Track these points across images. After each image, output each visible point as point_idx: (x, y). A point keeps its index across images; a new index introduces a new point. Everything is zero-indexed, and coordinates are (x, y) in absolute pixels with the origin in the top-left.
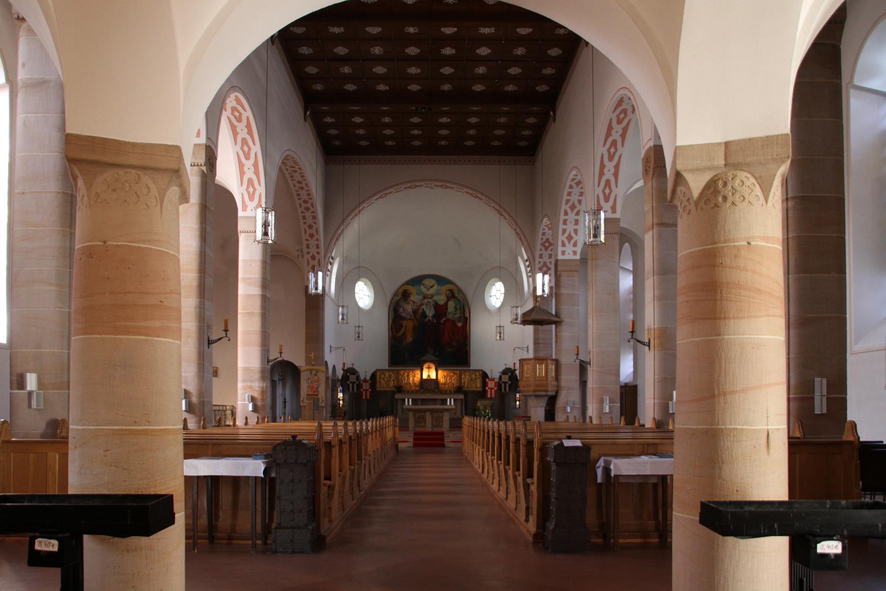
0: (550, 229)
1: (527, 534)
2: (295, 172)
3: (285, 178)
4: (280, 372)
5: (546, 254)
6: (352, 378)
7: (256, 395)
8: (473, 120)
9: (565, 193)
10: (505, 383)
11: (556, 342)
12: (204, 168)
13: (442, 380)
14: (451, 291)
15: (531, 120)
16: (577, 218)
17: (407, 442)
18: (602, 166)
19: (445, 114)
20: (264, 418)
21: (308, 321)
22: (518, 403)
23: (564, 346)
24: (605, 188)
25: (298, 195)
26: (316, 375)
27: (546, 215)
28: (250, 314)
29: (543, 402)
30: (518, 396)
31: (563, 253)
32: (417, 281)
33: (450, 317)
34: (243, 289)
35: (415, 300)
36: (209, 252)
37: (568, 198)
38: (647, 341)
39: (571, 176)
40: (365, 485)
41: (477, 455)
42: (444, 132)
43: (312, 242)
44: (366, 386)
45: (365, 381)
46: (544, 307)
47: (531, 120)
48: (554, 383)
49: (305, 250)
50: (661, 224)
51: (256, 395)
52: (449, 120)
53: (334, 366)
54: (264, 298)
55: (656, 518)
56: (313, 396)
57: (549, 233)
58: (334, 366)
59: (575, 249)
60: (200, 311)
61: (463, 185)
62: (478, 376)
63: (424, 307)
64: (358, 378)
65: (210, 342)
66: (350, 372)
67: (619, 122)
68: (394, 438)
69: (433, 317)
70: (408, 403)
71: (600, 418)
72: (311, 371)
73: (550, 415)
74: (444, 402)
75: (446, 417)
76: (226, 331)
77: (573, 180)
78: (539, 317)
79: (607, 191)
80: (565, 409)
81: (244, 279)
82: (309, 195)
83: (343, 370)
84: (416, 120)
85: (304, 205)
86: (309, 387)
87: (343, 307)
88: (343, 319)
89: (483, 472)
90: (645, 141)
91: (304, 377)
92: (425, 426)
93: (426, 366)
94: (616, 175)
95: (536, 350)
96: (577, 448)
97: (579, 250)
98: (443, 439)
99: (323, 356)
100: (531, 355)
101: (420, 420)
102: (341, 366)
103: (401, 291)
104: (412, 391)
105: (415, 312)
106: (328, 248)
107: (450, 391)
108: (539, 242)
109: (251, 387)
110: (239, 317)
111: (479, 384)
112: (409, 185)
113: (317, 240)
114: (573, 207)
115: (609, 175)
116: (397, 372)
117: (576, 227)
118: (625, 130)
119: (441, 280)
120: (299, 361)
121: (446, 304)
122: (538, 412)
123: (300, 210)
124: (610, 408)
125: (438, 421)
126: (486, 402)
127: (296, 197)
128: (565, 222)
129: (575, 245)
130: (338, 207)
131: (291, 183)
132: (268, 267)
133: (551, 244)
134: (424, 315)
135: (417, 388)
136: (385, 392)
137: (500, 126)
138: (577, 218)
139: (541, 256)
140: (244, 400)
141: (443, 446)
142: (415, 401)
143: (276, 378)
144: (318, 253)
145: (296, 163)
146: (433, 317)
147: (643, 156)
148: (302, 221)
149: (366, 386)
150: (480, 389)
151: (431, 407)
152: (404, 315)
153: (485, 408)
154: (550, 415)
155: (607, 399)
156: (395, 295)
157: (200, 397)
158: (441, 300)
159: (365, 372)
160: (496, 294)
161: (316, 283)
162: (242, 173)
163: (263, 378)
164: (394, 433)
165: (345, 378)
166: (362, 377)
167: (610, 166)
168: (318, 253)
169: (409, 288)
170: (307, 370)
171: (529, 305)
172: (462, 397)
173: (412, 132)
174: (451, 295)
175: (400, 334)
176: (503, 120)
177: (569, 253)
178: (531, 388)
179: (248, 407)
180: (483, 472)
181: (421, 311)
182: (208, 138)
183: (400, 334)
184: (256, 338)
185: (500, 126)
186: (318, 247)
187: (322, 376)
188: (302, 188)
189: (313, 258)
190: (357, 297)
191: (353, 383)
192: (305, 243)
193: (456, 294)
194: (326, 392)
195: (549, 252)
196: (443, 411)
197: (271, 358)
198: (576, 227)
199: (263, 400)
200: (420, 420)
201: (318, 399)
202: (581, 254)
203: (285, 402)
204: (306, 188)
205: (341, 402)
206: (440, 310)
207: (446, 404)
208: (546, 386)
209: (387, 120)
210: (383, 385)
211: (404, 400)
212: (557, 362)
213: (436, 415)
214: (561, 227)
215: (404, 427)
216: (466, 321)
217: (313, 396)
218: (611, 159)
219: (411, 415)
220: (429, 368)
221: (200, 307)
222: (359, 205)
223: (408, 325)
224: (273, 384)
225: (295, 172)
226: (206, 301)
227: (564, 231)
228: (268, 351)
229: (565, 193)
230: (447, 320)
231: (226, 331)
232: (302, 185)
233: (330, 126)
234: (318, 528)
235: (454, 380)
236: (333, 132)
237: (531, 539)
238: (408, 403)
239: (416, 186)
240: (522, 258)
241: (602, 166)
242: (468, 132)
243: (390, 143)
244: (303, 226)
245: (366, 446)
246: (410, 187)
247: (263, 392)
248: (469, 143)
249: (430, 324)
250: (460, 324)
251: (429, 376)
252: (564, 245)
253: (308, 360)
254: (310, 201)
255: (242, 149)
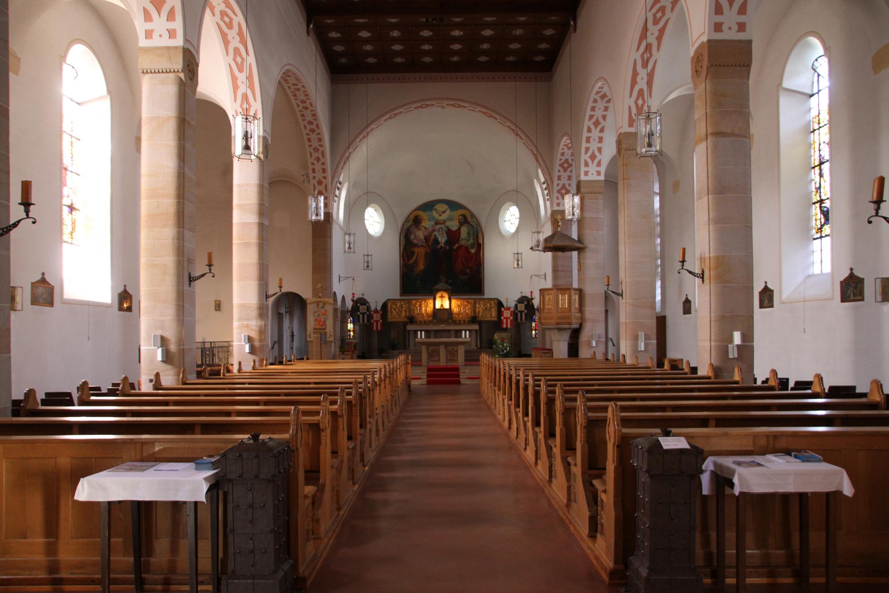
0: (569, 149)
1: (599, 569)
2: (298, 90)
3: (286, 94)
4: (285, 306)
5: (565, 175)
6: (363, 309)
7: (254, 335)
8: (488, 33)
9: (589, 108)
10: (521, 312)
11: (579, 270)
12: (182, 75)
13: (455, 309)
14: (464, 216)
15: (549, 32)
16: (601, 135)
17: (420, 382)
18: (635, 74)
19: (457, 26)
20: (261, 361)
21: (314, 250)
22: (534, 332)
23: (588, 273)
24: (637, 99)
25: (303, 115)
26: (323, 308)
27: (566, 134)
28: (247, 245)
29: (566, 336)
30: (534, 325)
31: (586, 173)
32: (429, 206)
33: (462, 243)
34: (238, 217)
35: (427, 226)
36: (189, 173)
37: (592, 113)
38: (697, 271)
39: (596, 89)
40: (370, 456)
41: (502, 405)
42: (456, 47)
43: (318, 167)
44: (377, 317)
45: (376, 311)
46: (565, 232)
47: (549, 32)
48: (579, 315)
49: (311, 175)
50: (717, 134)
51: (254, 335)
52: (462, 33)
53: (343, 297)
54: (261, 226)
55: (787, 544)
56: (321, 330)
57: (568, 153)
58: (343, 297)
59: (598, 169)
60: (179, 243)
61: (475, 103)
62: (493, 305)
63: (436, 233)
64: (368, 308)
65: (191, 279)
66: (360, 302)
67: (656, 22)
68: (406, 378)
69: (445, 244)
70: (421, 336)
71: (637, 357)
72: (318, 303)
73: (573, 350)
74: (458, 333)
75: (461, 351)
76: (210, 265)
77: (598, 93)
78: (558, 245)
79: (640, 102)
80: (590, 343)
81: (240, 206)
82: (314, 115)
83: (353, 301)
84: (426, 33)
85: (309, 127)
86: (316, 320)
87: (349, 234)
88: (350, 248)
89: (510, 428)
90: (696, 34)
91: (310, 309)
92: (439, 360)
93: (439, 295)
94: (650, 83)
95: (555, 277)
96: (682, 451)
97: (603, 169)
98: (458, 376)
99: (331, 287)
100: (549, 284)
101: (433, 354)
102: (351, 297)
103: (412, 217)
104: (425, 322)
105: (427, 239)
106: (335, 173)
107: (464, 321)
108: (558, 162)
109: (247, 326)
110: (235, 248)
111: (494, 313)
112: (419, 105)
113: (323, 164)
114: (597, 124)
115: (642, 84)
116: (409, 301)
117: (600, 145)
118: (662, 32)
119: (453, 205)
120: (306, 293)
121: (459, 229)
122: (561, 348)
123: (304, 132)
124: (646, 345)
125: (452, 355)
126: (504, 335)
127: (300, 119)
128: (588, 140)
129: (599, 165)
130: (345, 130)
131: (294, 102)
132: (266, 192)
133: (570, 165)
134: (436, 241)
135: (430, 319)
136: (398, 323)
137: (516, 39)
138: (601, 135)
139: (559, 178)
140: (240, 341)
141: (458, 382)
142: (428, 333)
143: (283, 311)
144: (325, 178)
145: (298, 80)
146: (445, 243)
147: (692, 54)
148: (307, 144)
149: (377, 317)
150: (496, 319)
151: (446, 340)
152: (415, 241)
153: (503, 341)
154: (573, 350)
155: (642, 335)
156: (407, 220)
157: (179, 345)
158: (454, 225)
159: (375, 302)
160: (510, 218)
161: (317, 208)
162: (235, 87)
163: (262, 314)
164: (406, 372)
165: (355, 308)
166: (373, 308)
167: (643, 73)
168: (325, 178)
169: (420, 213)
170: (313, 303)
171: (548, 231)
172: (476, 327)
173: (423, 47)
174: (464, 221)
175: (411, 262)
176: (518, 32)
177: (593, 173)
178: (554, 321)
179: (244, 347)
180: (510, 428)
181: (433, 237)
182: (186, 40)
183: (411, 262)
184: (253, 272)
185: (516, 39)
186: (324, 171)
187: (330, 309)
188: (306, 108)
189: (320, 183)
190: (367, 223)
191: (363, 314)
192: (311, 167)
193: (469, 219)
194: (334, 325)
195: (568, 173)
196: (457, 344)
197: (270, 293)
198: (600, 145)
199: (261, 340)
200: (433, 354)
201: (326, 334)
202: (606, 175)
203: (293, 336)
204: (310, 108)
205: (352, 333)
206: (453, 236)
207: (461, 337)
208: (569, 318)
209: (396, 34)
210: (394, 316)
211: (416, 332)
212: (580, 292)
213: (450, 348)
214: (584, 145)
215: (417, 363)
216: (479, 247)
217: (321, 330)
218: (645, 64)
219: (424, 348)
220: (442, 297)
221: (178, 239)
222: (367, 126)
223: (420, 252)
224: (279, 317)
225: (298, 90)
226: (187, 233)
227: (587, 149)
228: (267, 285)
229: (589, 108)
230: (460, 247)
231: (210, 265)
232: (306, 104)
233: (336, 41)
234: (295, 567)
235: (468, 310)
236: (339, 48)
237: (606, 578)
238: (421, 336)
239: (427, 106)
240: (539, 180)
241: (635, 74)
242: (481, 46)
243: (399, 60)
244: (308, 150)
245: (372, 404)
246: (421, 107)
247: (261, 332)
248: (483, 59)
249: (443, 253)
250: (473, 251)
251: (442, 305)
252: (586, 165)
253: (315, 292)
254: (315, 123)
255: (234, 60)
